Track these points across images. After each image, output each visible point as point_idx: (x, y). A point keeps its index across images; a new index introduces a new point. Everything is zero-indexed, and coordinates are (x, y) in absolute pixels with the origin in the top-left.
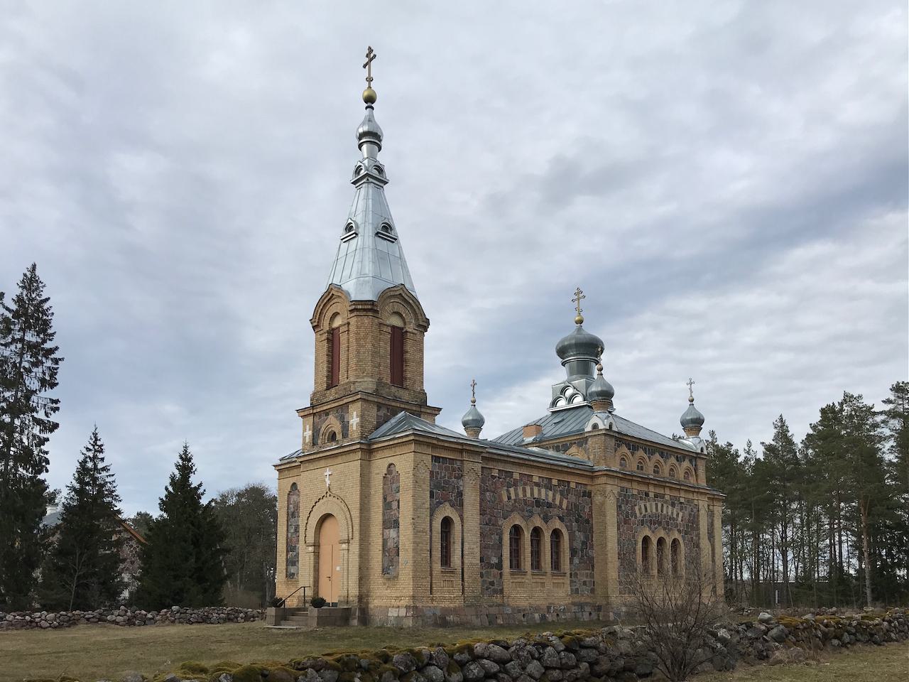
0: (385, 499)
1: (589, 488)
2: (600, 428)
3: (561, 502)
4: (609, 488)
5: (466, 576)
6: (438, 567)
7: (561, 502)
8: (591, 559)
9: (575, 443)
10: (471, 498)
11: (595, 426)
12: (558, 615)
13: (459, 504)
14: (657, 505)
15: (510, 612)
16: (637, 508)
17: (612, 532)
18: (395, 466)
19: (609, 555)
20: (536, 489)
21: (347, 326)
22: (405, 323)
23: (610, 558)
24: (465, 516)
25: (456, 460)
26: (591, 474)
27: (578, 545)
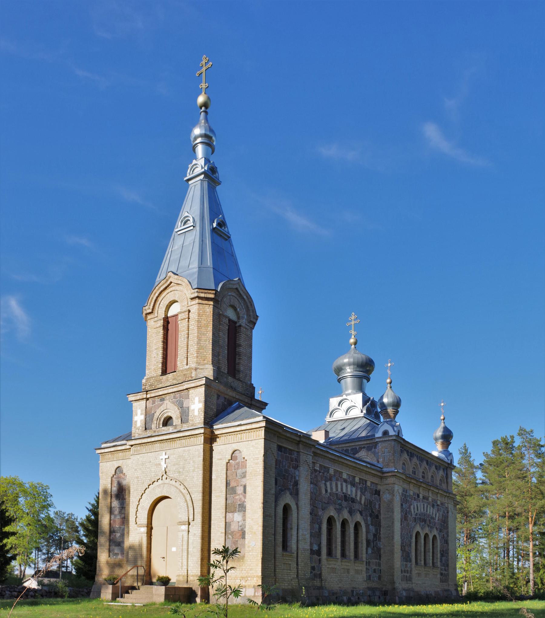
0: (227, 484)
1: (379, 487)
2: (390, 434)
3: (361, 499)
4: (396, 488)
5: (300, 560)
6: (280, 549)
7: (361, 499)
8: (379, 550)
9: (364, 447)
10: (305, 487)
11: (386, 433)
12: (359, 598)
13: (296, 494)
14: (424, 505)
15: (327, 595)
16: (412, 507)
17: (397, 526)
18: (240, 452)
19: (396, 546)
20: (344, 484)
21: (187, 313)
22: (239, 318)
23: (396, 549)
24: (300, 505)
25: (294, 451)
26: (379, 474)
27: (371, 537)
